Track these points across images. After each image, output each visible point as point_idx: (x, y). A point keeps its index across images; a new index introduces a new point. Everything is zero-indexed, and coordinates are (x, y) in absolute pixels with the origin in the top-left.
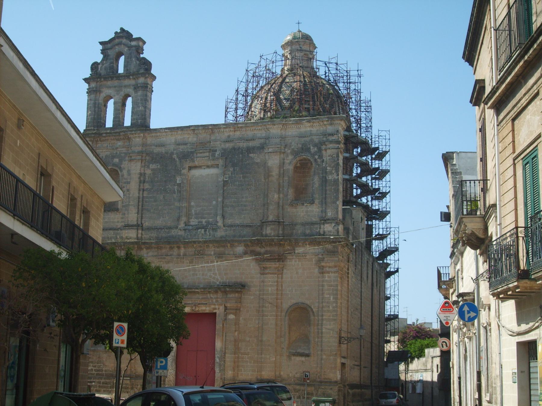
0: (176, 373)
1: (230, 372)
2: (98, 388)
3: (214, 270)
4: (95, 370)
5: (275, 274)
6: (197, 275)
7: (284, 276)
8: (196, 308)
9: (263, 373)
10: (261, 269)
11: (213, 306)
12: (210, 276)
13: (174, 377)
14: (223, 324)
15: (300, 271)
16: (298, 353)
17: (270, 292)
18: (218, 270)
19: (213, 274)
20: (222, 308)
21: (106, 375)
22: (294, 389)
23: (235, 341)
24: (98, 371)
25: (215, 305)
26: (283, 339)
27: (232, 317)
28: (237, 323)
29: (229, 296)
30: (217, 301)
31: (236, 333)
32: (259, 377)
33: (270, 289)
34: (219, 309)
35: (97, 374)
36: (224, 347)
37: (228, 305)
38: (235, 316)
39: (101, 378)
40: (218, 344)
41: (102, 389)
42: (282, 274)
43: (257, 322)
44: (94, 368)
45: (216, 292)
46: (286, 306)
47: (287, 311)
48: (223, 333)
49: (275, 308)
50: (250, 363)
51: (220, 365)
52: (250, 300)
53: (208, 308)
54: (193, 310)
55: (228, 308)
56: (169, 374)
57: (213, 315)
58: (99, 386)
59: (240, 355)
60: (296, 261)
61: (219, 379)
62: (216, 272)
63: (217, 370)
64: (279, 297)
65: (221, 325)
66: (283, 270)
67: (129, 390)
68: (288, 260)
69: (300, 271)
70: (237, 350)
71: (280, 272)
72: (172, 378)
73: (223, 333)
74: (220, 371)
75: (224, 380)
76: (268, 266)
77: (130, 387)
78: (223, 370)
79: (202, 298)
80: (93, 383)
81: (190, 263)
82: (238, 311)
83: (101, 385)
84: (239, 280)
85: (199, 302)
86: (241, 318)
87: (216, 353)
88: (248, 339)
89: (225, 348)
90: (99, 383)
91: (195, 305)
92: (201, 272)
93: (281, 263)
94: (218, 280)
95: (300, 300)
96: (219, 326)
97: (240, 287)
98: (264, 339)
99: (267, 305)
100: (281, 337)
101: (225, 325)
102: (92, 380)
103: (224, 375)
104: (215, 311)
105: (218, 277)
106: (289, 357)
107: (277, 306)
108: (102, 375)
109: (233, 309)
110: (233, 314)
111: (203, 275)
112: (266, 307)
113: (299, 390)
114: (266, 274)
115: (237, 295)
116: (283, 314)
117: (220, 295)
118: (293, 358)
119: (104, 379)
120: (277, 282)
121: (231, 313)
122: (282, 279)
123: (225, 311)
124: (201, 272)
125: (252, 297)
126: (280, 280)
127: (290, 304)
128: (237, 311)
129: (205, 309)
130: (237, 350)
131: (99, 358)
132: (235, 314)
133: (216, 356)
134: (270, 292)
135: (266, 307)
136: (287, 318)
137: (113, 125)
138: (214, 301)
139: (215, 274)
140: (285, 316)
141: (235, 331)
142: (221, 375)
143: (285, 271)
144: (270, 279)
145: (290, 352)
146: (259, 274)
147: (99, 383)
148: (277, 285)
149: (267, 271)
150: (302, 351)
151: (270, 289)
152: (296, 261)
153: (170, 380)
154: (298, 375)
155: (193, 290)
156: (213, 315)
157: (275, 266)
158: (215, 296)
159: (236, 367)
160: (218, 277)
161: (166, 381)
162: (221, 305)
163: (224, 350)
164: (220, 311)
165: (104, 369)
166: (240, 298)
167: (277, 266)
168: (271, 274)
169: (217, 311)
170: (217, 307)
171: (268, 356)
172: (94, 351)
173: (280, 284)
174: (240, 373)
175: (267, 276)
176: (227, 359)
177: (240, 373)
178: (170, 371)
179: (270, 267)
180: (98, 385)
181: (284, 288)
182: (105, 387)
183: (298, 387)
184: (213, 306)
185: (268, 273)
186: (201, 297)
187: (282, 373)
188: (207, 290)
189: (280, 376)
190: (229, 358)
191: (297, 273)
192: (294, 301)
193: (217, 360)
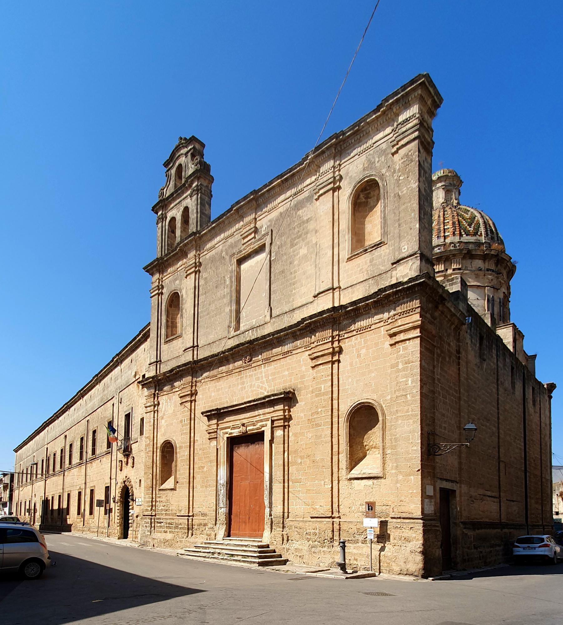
104: (263, 429)
105: (266, 386)
139: (263, 383)
160: (266, 386)
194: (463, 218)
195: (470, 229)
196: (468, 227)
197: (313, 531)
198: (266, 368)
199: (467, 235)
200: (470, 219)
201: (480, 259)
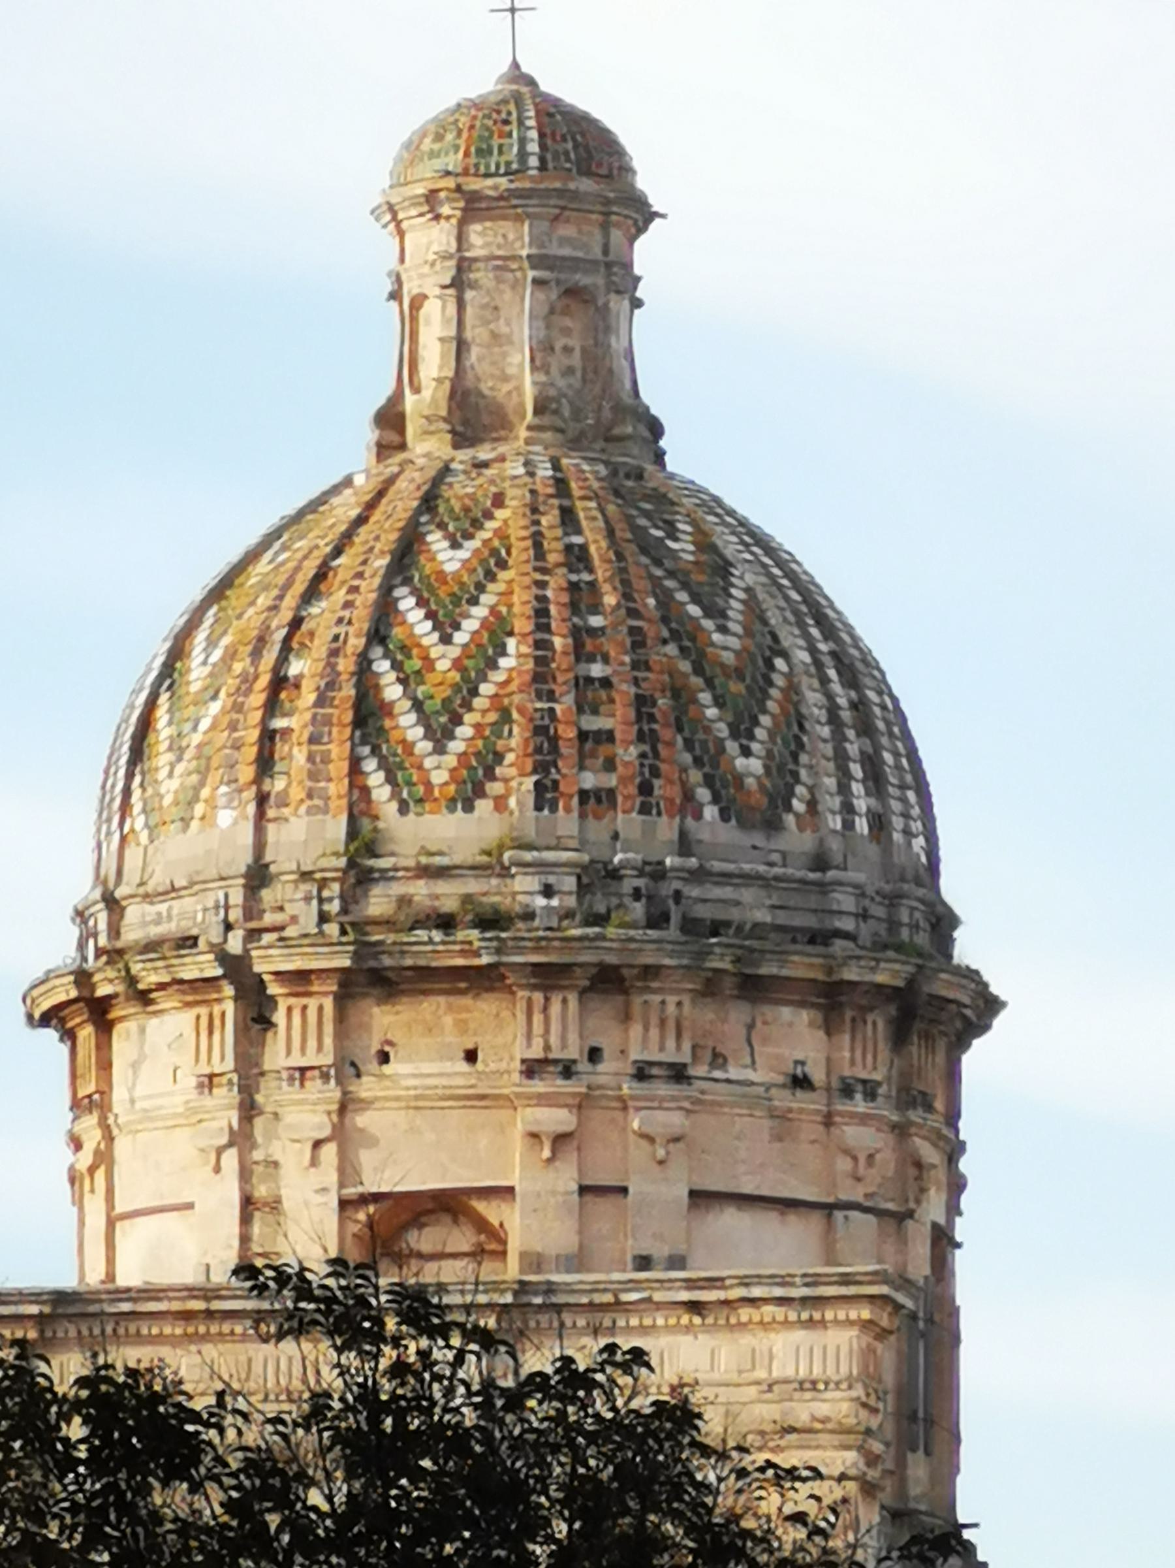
194: (698, 670)
195: (740, 763)
196: (732, 747)
199: (725, 816)
200: (739, 674)
201: (802, 1004)
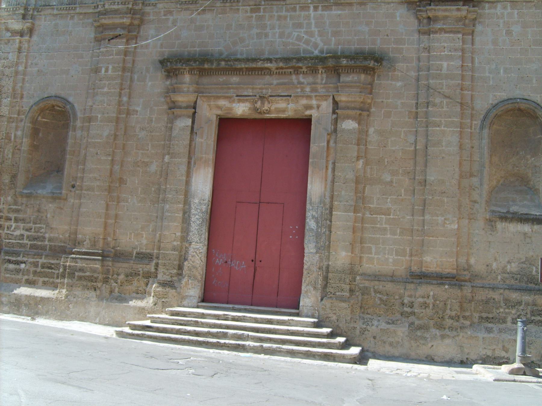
0: (208, 249)
1: (344, 254)
2: (31, 277)
3: (309, 24)
4: (28, 237)
5: (459, 32)
6: (266, 36)
7: (477, 39)
8: (263, 103)
9: (427, 258)
10: (420, 21)
11: (304, 102)
12: (299, 39)
13: (204, 259)
14: (328, 142)
15: (516, 29)
16: (514, 213)
17: (444, 71)
18: (316, 27)
19: (306, 33)
20: (327, 106)
21: (50, 249)
22: (507, 301)
23: (357, 181)
24: (35, 239)
25: (309, 97)
26: (475, 181)
27: (349, 125)
28: (361, 139)
29: (346, 78)
30: (314, 90)
31: (361, 162)
32: (415, 268)
33: (445, 64)
34: (318, 107)
35: (32, 247)
36: (328, 194)
37: (343, 98)
38: (359, 124)
39: (40, 256)
40: (316, 188)
41: (42, 279)
42: (472, 33)
43: (411, 139)
44: (26, 233)
45: (313, 71)
46: (483, 103)
47: (485, 118)
48: (327, 161)
49: (458, 109)
50: (394, 234)
51: (318, 236)
52: (394, 91)
53: (292, 106)
54: (256, 110)
55: (341, 105)
56: (191, 251)
57: (305, 124)
58: (35, 273)
59: (368, 215)
60: (505, 8)
61: (315, 269)
62: (313, 28)
63: (310, 247)
64: (467, 83)
65: (325, 144)
66: (474, 25)
67: (99, 285)
68: (487, 5)
69: (516, 29)
70: (360, 203)
71: (467, 28)
72: (198, 262)
73: (327, 161)
74: (318, 250)
75: (328, 271)
76: (440, 14)
77: (101, 277)
78: (325, 248)
79: (278, 84)
80: (23, 266)
81: (252, 11)
82: (365, 113)
83: (39, 269)
84: (367, 47)
85: (270, 92)
86: (371, 130)
87: (308, 206)
88: (387, 177)
89: (332, 197)
90: (36, 265)
91: (262, 98)
92: (277, 30)
93: (472, 9)
94: (316, 46)
95: (518, 93)
96: (317, 146)
97: (369, 62)
98: (431, 178)
99: (438, 100)
100: (471, 175)
101: (332, 144)
102: (20, 259)
103: (328, 259)
104: (308, 113)
105: (318, 39)
106: (490, 223)
107: (461, 104)
108: (43, 248)
109: (354, 109)
110: (353, 118)
111: (282, 35)
112: (434, 105)
113: (520, 303)
114: (435, 32)
115: (363, 76)
116: (477, 123)
117: (321, 77)
118: (500, 225)
119: (47, 256)
120: (463, 50)
121: (348, 117)
122: (473, 44)
123: (334, 112)
124: (277, 30)
125: (399, 84)
126: (468, 46)
127: (492, 100)
128: (363, 112)
129: (285, 108)
130: (360, 203)
131: (39, 211)
132: (359, 120)
133: (309, 214)
134: (444, 71)
135: (434, 105)
136: (486, 131)
137: (368, 360)
138: (308, 89)
139: (311, 34)
140: (482, 128)
141: (358, 158)
142: (321, 260)
143: (479, 28)
144: (445, 44)
145: (493, 211)
146: (416, 36)
147: (36, 265)
148: (463, 58)
149: (438, 26)
150: (524, 211)
151: (445, 64)
152: (505, 8)
153: (194, 267)
154: (513, 267)
155: (259, 64)
156: (305, 124)
157: (459, 14)
158: (310, 79)
159: (358, 243)
160: (318, 39)
161: (185, 268)
162: (324, 98)
163: (328, 200)
164: (320, 112)
165: (47, 236)
166: (371, 84)
167: (464, 13)
168: (446, 32)
169: (314, 113)
170: (314, 102)
171: (440, 219)
172: (29, 196)
173: (468, 55)
174: (365, 256)
175: (437, 36)
176: (336, 223)
177: (365, 256)
178: (194, 245)
179: (446, 17)
180: (32, 269)
181: (477, 65)
182: (46, 275)
183: (515, 296)
184: (304, 102)
185: (441, 30)
186: (275, 82)
187: (472, 261)
188: (294, 63)
189: (469, 268)
190: (342, 218)
191: (509, 33)
192: (504, 95)
193: (311, 224)
197: (421, 300)
198: (320, 12)
